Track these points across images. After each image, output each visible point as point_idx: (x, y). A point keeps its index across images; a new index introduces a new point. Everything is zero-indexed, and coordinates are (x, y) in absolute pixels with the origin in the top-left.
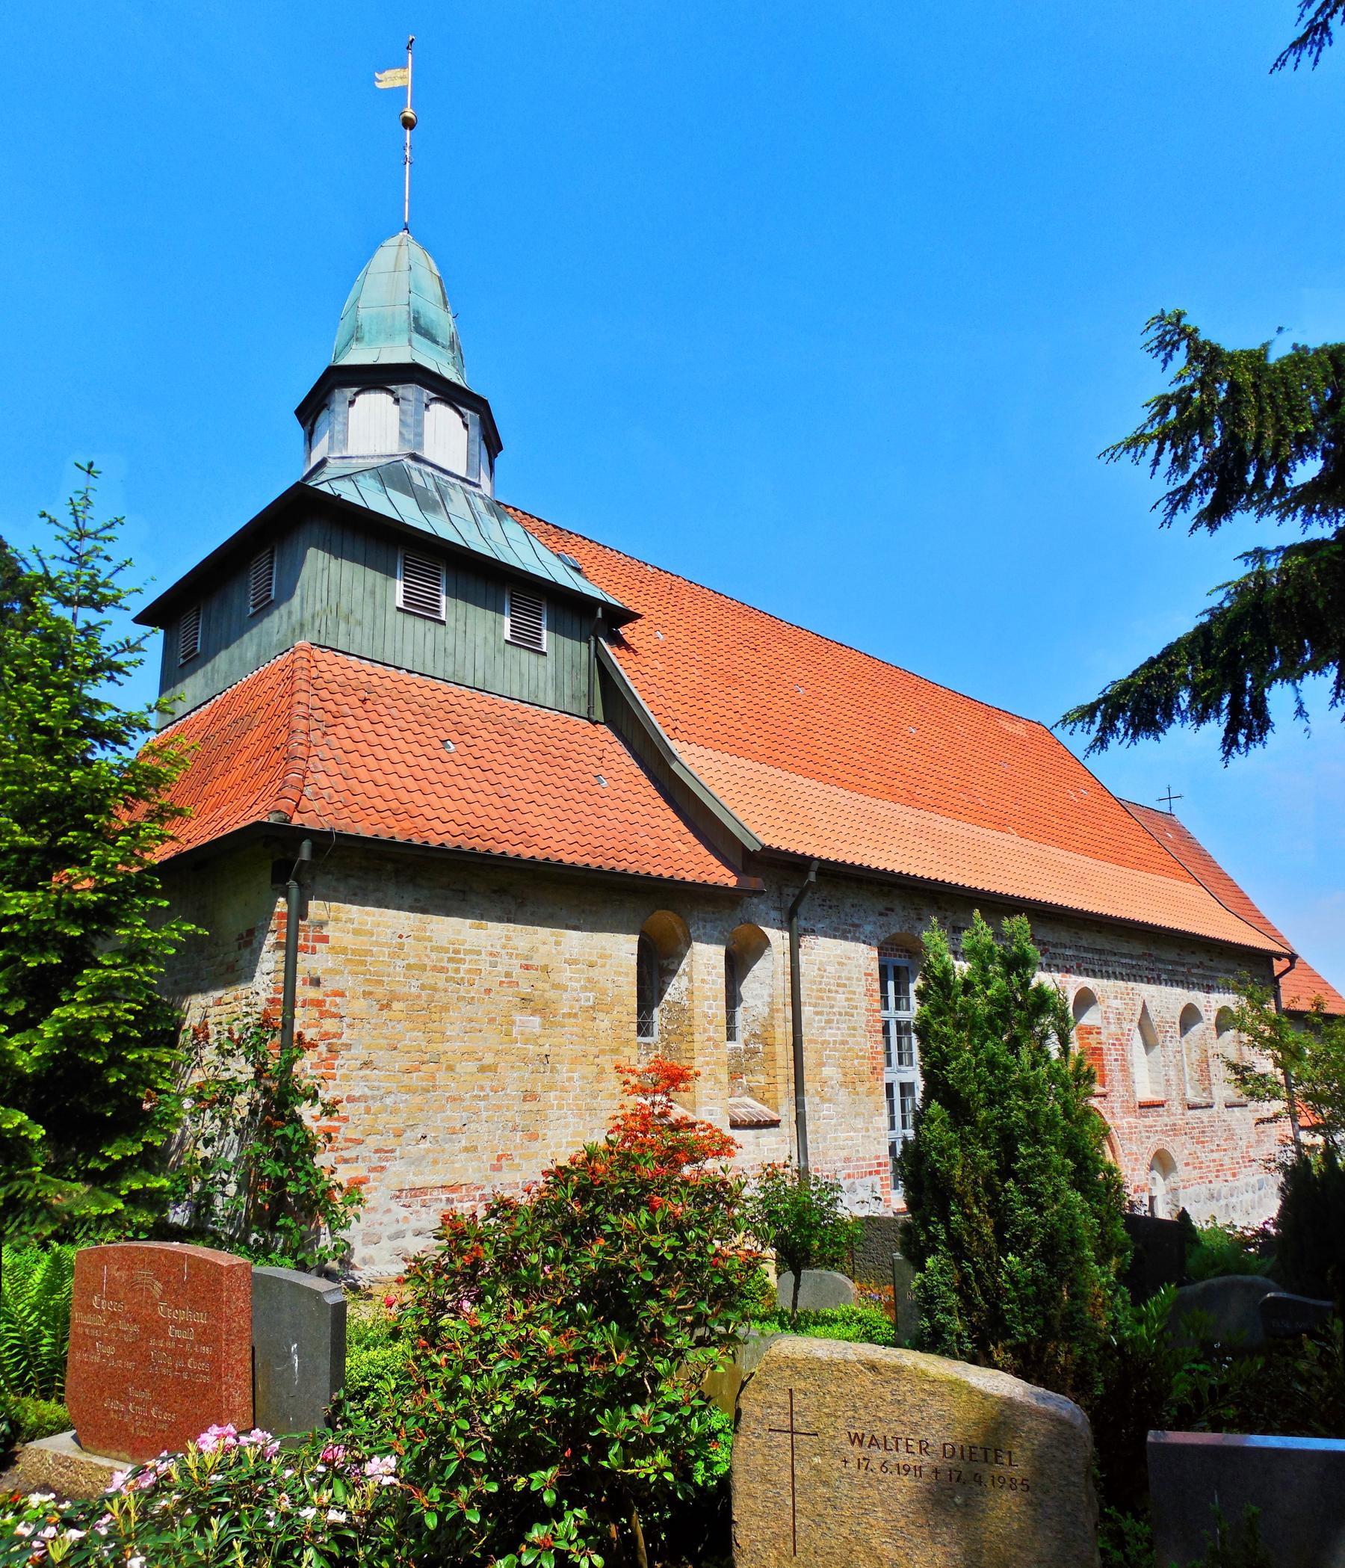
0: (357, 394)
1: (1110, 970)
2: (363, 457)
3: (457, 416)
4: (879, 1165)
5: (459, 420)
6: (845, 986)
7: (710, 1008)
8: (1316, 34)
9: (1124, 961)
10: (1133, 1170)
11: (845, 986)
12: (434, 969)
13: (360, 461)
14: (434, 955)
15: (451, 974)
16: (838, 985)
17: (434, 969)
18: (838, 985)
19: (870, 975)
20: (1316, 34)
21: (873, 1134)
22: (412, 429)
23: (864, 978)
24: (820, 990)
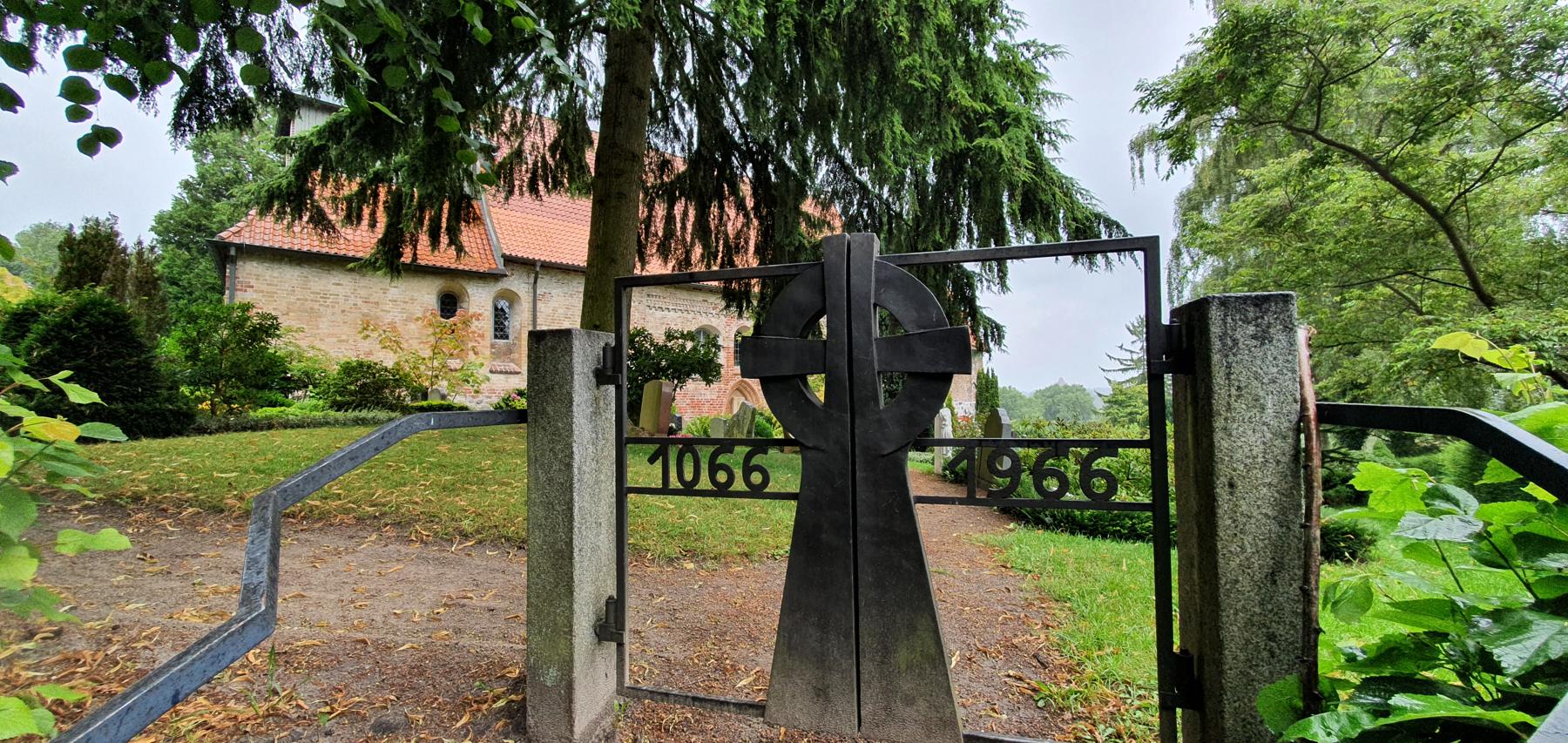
8: (1192, 1)
12: (312, 301)
17: (312, 301)
20: (1192, 1)
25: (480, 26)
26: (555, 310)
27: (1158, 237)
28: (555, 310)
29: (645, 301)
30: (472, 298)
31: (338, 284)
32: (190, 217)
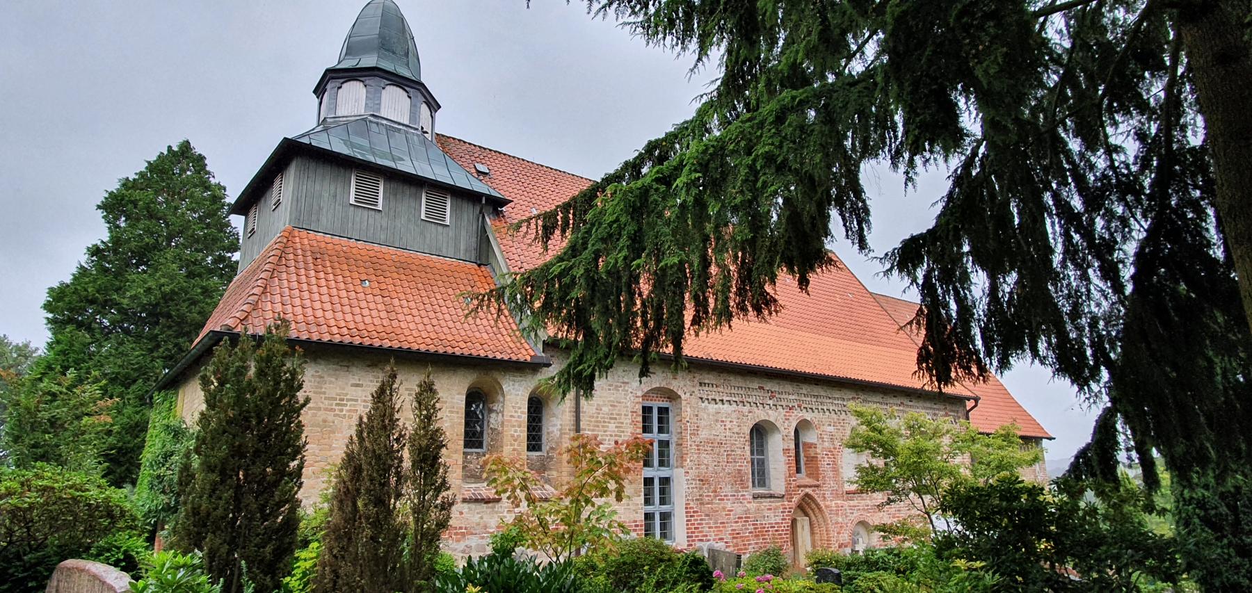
0: (343, 83)
1: (825, 408)
2: (346, 117)
3: (404, 92)
4: (637, 526)
5: (405, 94)
6: (616, 419)
7: (516, 431)
8: (568, 1)
9: (836, 402)
10: (839, 533)
11: (616, 419)
12: (326, 409)
13: (345, 119)
14: (326, 402)
15: (337, 412)
16: (611, 418)
17: (326, 409)
18: (611, 418)
19: (636, 412)
20: (568, 1)
21: (632, 507)
22: (375, 100)
23: (630, 414)
24: (597, 422)
25: (1213, 231)
26: (599, 409)
27: (185, 152)
28: (599, 409)
29: (697, 392)
30: (508, 397)
31: (357, 385)
32: (98, 292)
